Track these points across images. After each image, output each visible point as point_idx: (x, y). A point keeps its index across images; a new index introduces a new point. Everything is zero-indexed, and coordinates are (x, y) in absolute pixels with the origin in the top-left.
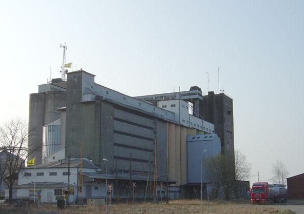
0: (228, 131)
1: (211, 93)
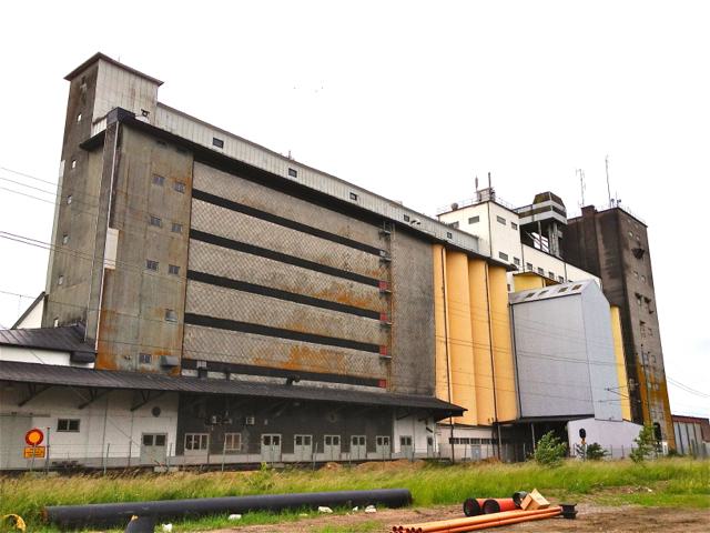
0: (638, 297)
1: (588, 210)
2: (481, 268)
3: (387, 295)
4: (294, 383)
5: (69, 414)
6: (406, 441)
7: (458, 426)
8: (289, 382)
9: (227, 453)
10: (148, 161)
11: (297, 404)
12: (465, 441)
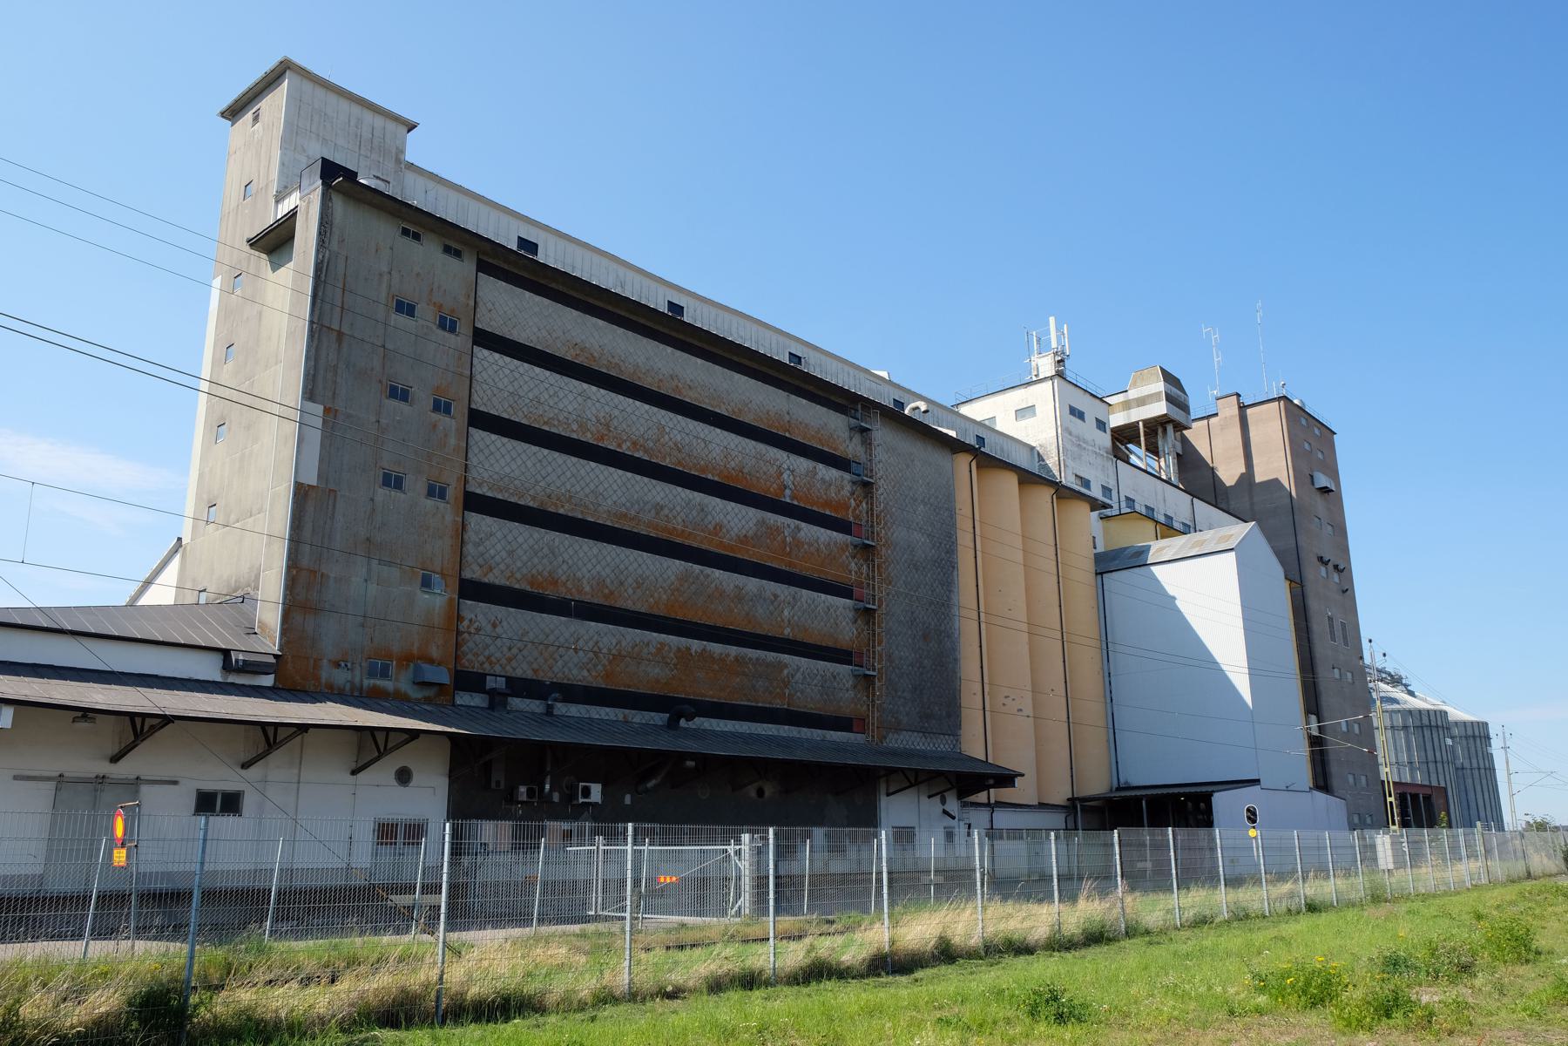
2: (1045, 495)
3: (866, 551)
4: (683, 723)
5: (222, 778)
6: (904, 836)
7: (1001, 804)
8: (672, 724)
9: (541, 921)
10: (385, 269)
11: (690, 764)
12: (1015, 834)
